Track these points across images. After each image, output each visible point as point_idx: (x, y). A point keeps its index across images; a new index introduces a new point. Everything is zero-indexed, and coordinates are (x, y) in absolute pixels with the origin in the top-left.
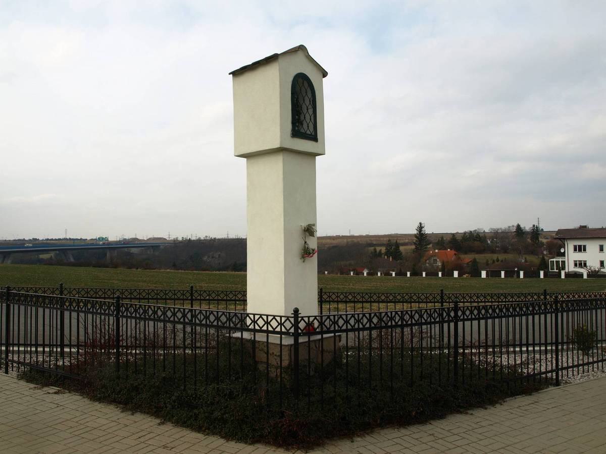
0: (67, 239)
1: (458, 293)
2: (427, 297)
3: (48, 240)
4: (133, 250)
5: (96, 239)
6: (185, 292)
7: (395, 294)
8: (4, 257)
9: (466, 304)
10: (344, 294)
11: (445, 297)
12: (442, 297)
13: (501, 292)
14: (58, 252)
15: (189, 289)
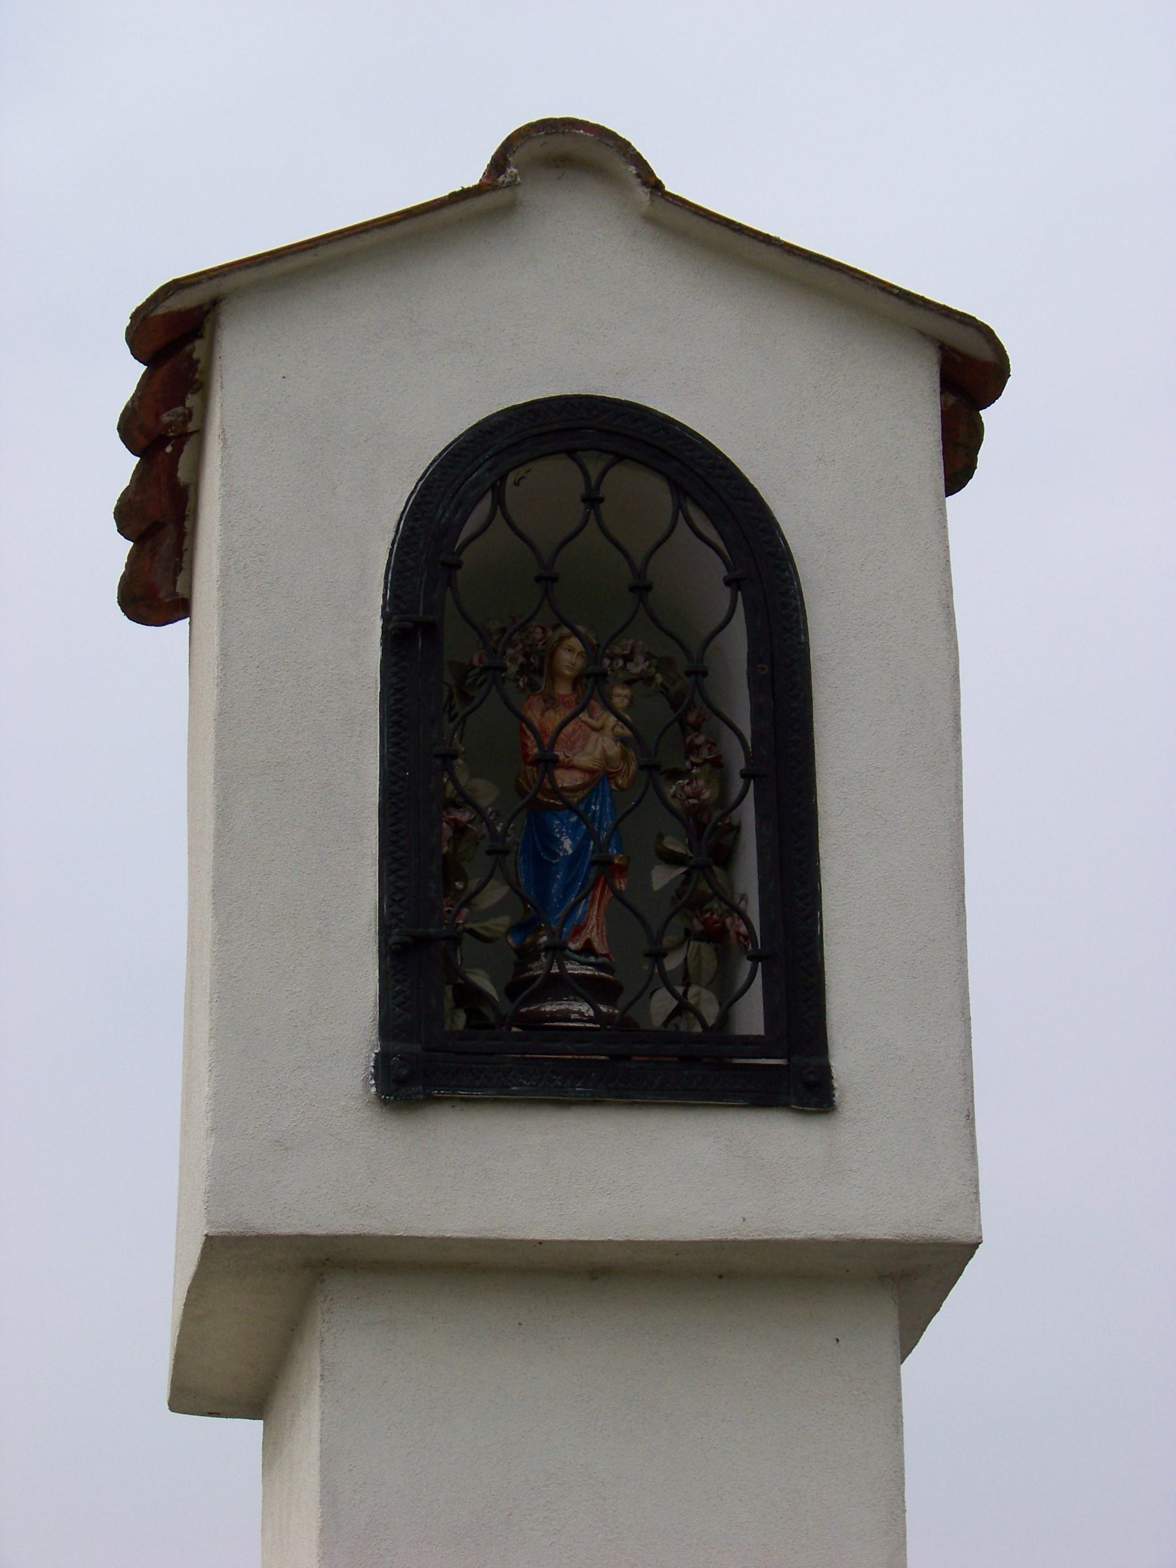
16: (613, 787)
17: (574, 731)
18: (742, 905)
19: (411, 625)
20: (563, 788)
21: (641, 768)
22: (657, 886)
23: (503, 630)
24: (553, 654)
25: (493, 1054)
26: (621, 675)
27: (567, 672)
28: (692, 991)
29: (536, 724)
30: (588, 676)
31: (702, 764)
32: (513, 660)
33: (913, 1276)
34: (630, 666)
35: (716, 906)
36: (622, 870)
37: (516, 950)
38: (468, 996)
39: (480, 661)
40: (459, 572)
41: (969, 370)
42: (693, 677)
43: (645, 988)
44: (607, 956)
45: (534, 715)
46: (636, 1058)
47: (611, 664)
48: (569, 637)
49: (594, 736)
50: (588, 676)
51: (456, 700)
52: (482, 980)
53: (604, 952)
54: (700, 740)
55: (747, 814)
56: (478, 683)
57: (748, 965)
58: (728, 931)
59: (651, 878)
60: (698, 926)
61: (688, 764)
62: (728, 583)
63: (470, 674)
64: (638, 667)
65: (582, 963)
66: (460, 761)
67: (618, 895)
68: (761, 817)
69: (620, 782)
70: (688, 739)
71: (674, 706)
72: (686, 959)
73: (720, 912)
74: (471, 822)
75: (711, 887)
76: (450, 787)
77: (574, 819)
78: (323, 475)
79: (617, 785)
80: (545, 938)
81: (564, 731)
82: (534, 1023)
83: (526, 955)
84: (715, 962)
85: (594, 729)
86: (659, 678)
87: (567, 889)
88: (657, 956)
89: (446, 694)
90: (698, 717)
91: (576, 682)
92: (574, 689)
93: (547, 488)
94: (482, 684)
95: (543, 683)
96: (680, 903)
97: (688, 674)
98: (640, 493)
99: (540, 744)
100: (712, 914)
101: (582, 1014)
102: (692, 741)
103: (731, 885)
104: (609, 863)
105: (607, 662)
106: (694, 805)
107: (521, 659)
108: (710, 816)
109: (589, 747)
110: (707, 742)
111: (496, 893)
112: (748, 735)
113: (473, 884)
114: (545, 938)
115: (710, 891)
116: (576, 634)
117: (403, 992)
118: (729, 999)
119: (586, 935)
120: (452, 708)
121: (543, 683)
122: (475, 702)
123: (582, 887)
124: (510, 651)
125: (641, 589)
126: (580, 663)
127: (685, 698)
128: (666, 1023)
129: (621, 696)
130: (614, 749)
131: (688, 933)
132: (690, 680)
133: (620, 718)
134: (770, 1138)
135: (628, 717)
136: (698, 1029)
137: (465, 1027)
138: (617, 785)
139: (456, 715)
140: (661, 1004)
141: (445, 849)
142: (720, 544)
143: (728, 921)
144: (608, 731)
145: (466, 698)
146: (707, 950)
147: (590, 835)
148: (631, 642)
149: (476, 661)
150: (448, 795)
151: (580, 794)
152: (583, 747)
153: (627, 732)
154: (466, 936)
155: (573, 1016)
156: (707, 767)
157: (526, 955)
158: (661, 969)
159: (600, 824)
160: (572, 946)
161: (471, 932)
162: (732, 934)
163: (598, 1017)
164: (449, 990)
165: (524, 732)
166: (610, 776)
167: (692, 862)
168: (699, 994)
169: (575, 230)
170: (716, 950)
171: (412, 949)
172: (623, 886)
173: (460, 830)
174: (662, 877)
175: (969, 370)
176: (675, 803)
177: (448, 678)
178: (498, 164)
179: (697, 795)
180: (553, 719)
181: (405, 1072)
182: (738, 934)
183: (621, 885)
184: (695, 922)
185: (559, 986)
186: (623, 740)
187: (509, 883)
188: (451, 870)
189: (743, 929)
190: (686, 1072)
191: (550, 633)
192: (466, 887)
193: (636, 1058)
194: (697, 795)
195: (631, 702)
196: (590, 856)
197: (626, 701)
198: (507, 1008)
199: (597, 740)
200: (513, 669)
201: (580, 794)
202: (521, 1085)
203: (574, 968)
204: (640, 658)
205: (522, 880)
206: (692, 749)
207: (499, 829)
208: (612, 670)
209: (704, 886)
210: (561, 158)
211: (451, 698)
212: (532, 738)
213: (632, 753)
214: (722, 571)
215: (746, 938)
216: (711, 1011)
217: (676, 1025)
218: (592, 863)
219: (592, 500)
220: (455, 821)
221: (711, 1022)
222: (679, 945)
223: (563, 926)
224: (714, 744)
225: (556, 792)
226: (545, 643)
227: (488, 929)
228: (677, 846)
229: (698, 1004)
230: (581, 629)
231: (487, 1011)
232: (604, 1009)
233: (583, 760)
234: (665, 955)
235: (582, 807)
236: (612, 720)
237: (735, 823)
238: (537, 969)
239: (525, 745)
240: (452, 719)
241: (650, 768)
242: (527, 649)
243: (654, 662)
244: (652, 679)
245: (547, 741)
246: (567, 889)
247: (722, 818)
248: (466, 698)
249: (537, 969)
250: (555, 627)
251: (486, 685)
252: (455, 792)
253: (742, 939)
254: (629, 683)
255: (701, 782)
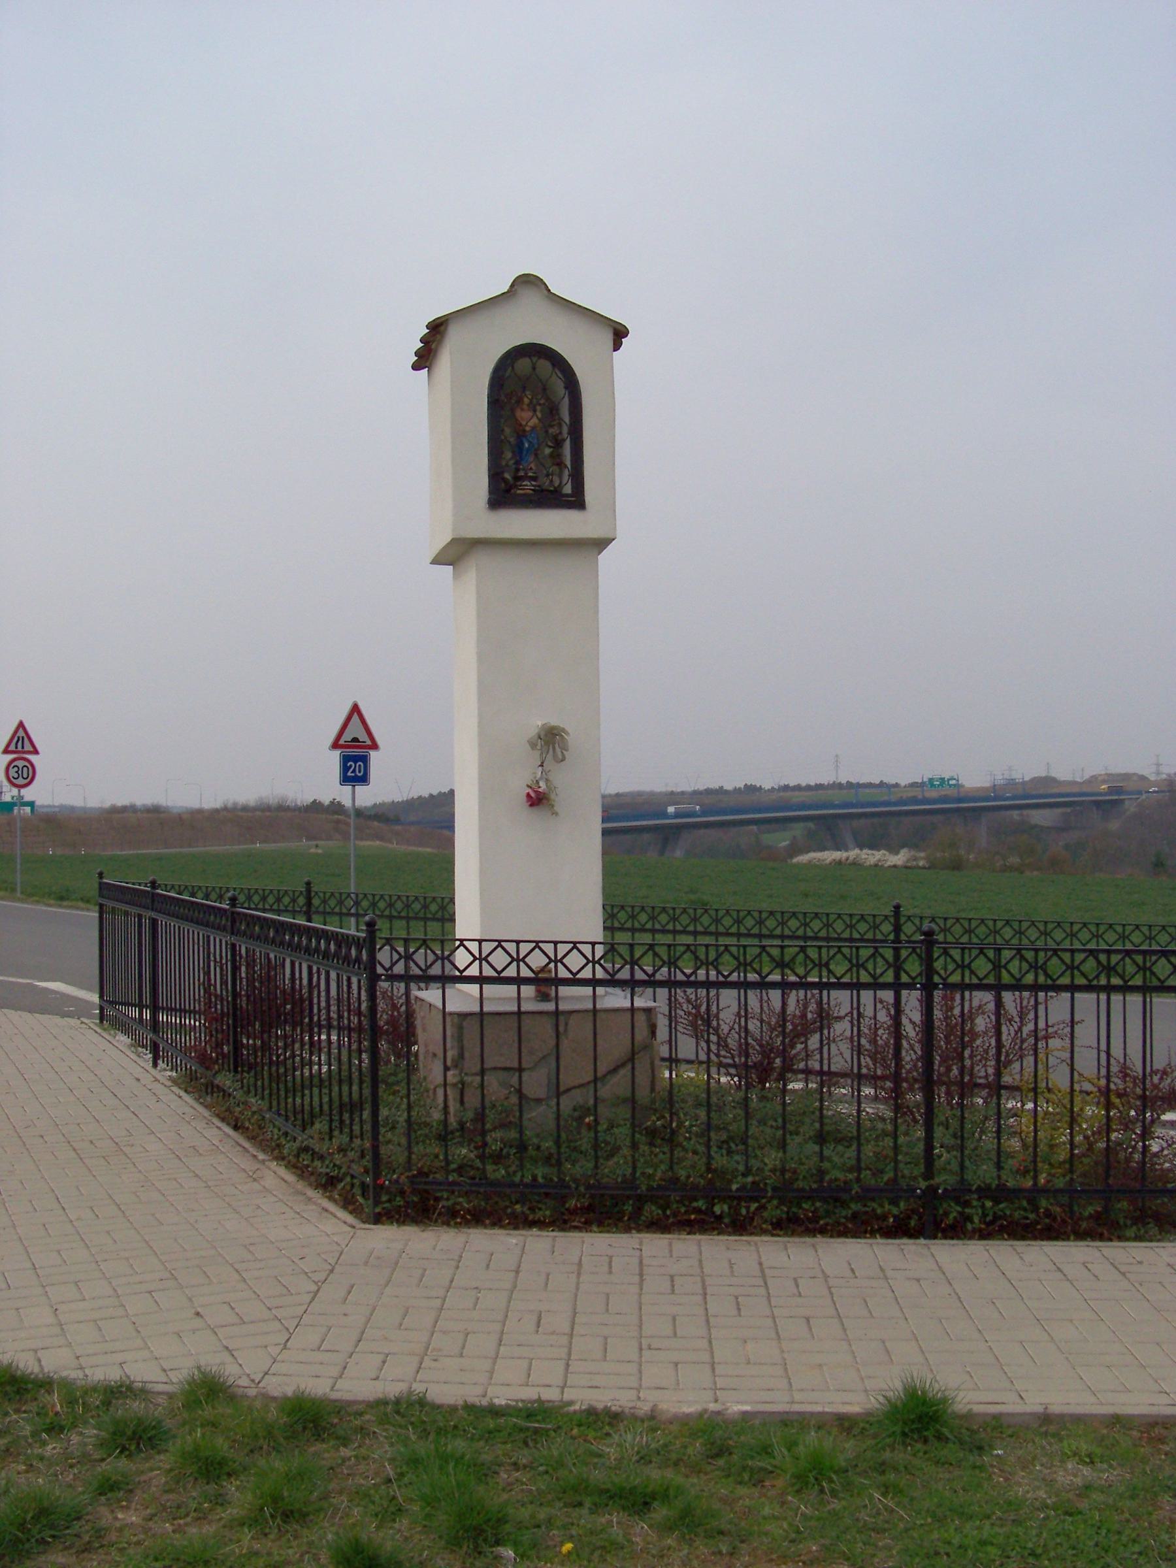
0: (839, 786)
1: (833, 911)
2: (1021, 933)
3: (786, 788)
4: (1041, 818)
5: (923, 784)
6: (1131, 928)
7: (946, 919)
8: (666, 841)
9: (658, 936)
10: (845, 917)
11: (316, 902)
12: (309, 903)
13: (255, 885)
14: (811, 825)
15: (888, 911)
33: (601, 544)
41: (619, 334)
78: (473, 359)
83: (518, 470)
93: (523, 365)
98: (544, 366)
127: (552, 410)
134: (572, 515)
142: (567, 445)
169: (529, 297)
171: (495, 475)
175: (619, 334)
178: (512, 285)
210: (527, 282)
219: (534, 369)
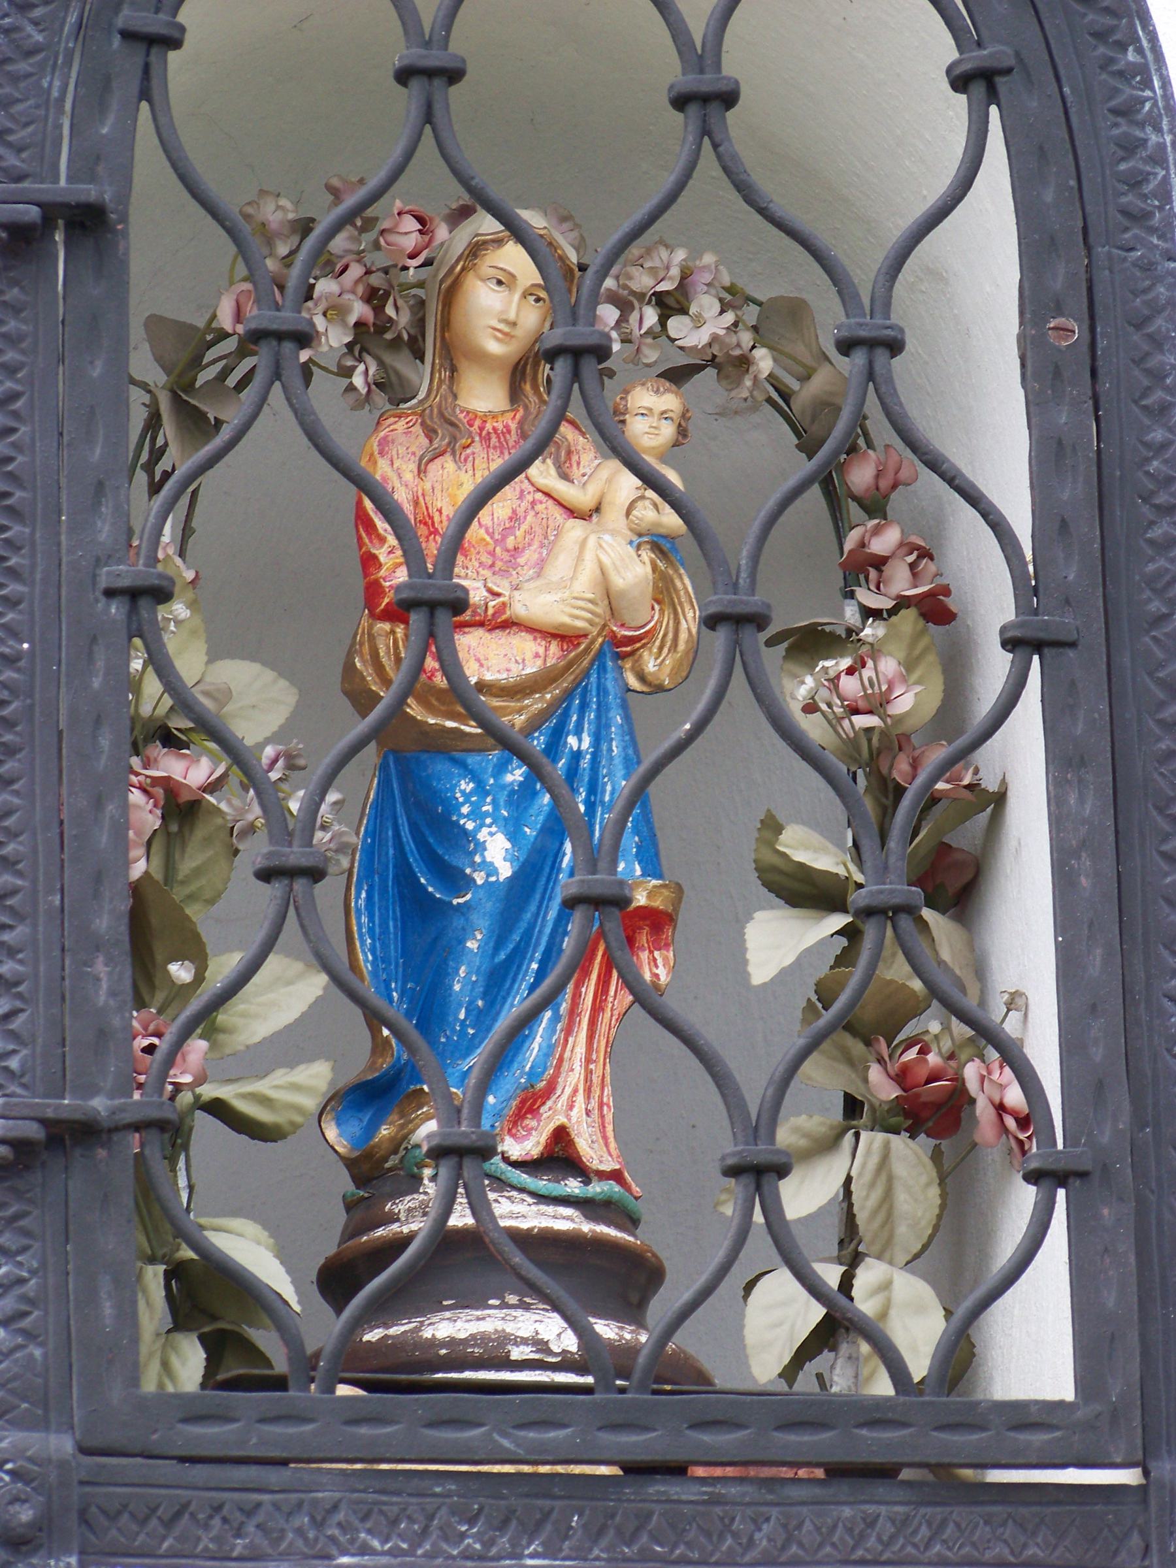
16: (633, 682)
17: (514, 517)
18: (1011, 1026)
19: (34, 213)
20: (481, 686)
21: (711, 622)
22: (761, 970)
23: (304, 227)
24: (451, 294)
25: (284, 1463)
26: (651, 355)
27: (494, 347)
28: (867, 1276)
29: (402, 496)
30: (552, 355)
31: (893, 612)
32: (335, 311)
34: (676, 325)
35: (935, 1027)
36: (657, 922)
37: (351, 1164)
38: (208, 1297)
39: (238, 317)
40: (172, 55)
42: (859, 357)
43: (724, 1270)
44: (616, 1176)
45: (398, 469)
46: (700, 1472)
47: (622, 320)
48: (499, 242)
49: (575, 530)
50: (552, 355)
51: (169, 430)
52: (249, 1249)
53: (609, 1165)
54: (885, 542)
55: (1021, 758)
56: (231, 381)
57: (1026, 1196)
58: (973, 1101)
59: (742, 949)
60: (882, 1088)
61: (851, 614)
62: (960, 81)
63: (210, 355)
64: (694, 332)
65: (542, 1198)
66: (179, 608)
67: (646, 999)
68: (1063, 759)
69: (651, 666)
70: (850, 543)
71: (809, 448)
72: (849, 1180)
73: (947, 1045)
74: (213, 787)
75: (918, 972)
76: (152, 687)
77: (516, 775)
79: (642, 677)
80: (432, 1126)
81: (484, 515)
82: (402, 1377)
84: (934, 1192)
85: (572, 512)
86: (764, 362)
87: (497, 981)
88: (760, 1174)
89: (138, 417)
90: (879, 475)
91: (519, 374)
92: (515, 394)
94: (241, 385)
95: (422, 378)
96: (827, 1016)
97: (846, 346)
99: (412, 556)
100: (923, 1051)
101: (542, 1345)
102: (862, 545)
103: (980, 970)
104: (608, 901)
105: (609, 314)
106: (869, 730)
107: (359, 310)
108: (915, 765)
109: (560, 566)
110: (907, 547)
111: (286, 994)
112: (1022, 525)
113: (224, 965)
114: (432, 1126)
115: (917, 985)
116: (517, 232)
117: (21, 1281)
118: (973, 1294)
119: (552, 1116)
120: (158, 454)
121: (422, 378)
122: (225, 434)
123: (541, 975)
124: (325, 286)
125: (707, 100)
126: (531, 318)
128: (790, 1372)
129: (651, 415)
130: (634, 571)
131: (852, 1106)
132: (851, 365)
133: (650, 480)
135: (673, 477)
136: (883, 1387)
137: (203, 1386)
138: (642, 677)
139: (167, 475)
140: (775, 1318)
141: (138, 869)
143: (971, 1072)
144: (614, 516)
145: (197, 424)
146: (909, 1156)
147: (557, 826)
148: (680, 255)
149: (226, 320)
150: (146, 710)
151: (536, 704)
152: (541, 565)
153: (671, 520)
154: (202, 1120)
155: (517, 1353)
156: (908, 619)
157: (375, 1176)
158: (773, 1211)
159: (594, 788)
160: (514, 1148)
161: (218, 1109)
162: (983, 1109)
163: (591, 1356)
164: (154, 1276)
165: (370, 526)
166: (622, 648)
167: (857, 899)
168: (886, 1286)
170: (936, 1156)
172: (662, 972)
173: (181, 810)
174: (780, 944)
176: (813, 728)
177: (144, 364)
179: (878, 704)
180: (452, 483)
181: (25, 1514)
182: (1001, 1108)
183: (656, 967)
184: (875, 1073)
185: (465, 1262)
186: (659, 544)
187: (326, 967)
188: (151, 931)
189: (1014, 1096)
190: (847, 1512)
191: (442, 232)
192: (199, 978)
193: (700, 1472)
194: (878, 704)
195: (682, 431)
196: (566, 883)
197: (668, 431)
198: (322, 1328)
199: (583, 544)
200: (335, 338)
201: (536, 704)
202: (365, 1550)
203: (516, 1212)
204: (705, 304)
205: (365, 960)
206: (864, 567)
207: (294, 806)
208: (626, 340)
209: (897, 970)
211: (154, 422)
212: (392, 540)
213: (685, 584)
214: (945, 50)
215: (1023, 1122)
216: (919, 1334)
217: (819, 1377)
218: (570, 904)
220: (169, 787)
221: (919, 1367)
222: (827, 1145)
223: (484, 1087)
224: (925, 554)
225: (460, 696)
226: (428, 263)
227: (264, 1101)
228: (816, 851)
229: (884, 1314)
230: (534, 219)
231: (265, 1339)
232: (606, 1329)
233: (542, 602)
234: (782, 1171)
235: (539, 742)
236: (629, 483)
237: (991, 784)
238: (410, 1218)
239: (369, 561)
240: (155, 488)
241: (733, 621)
242: (376, 280)
243: (751, 314)
244: (744, 362)
245: (432, 548)
246: (497, 981)
247: (944, 768)
248: (197, 424)
249: (410, 1218)
250: (462, 214)
251: (249, 395)
252: (168, 701)
253: (1010, 1122)
254: (677, 376)
255: (889, 666)
